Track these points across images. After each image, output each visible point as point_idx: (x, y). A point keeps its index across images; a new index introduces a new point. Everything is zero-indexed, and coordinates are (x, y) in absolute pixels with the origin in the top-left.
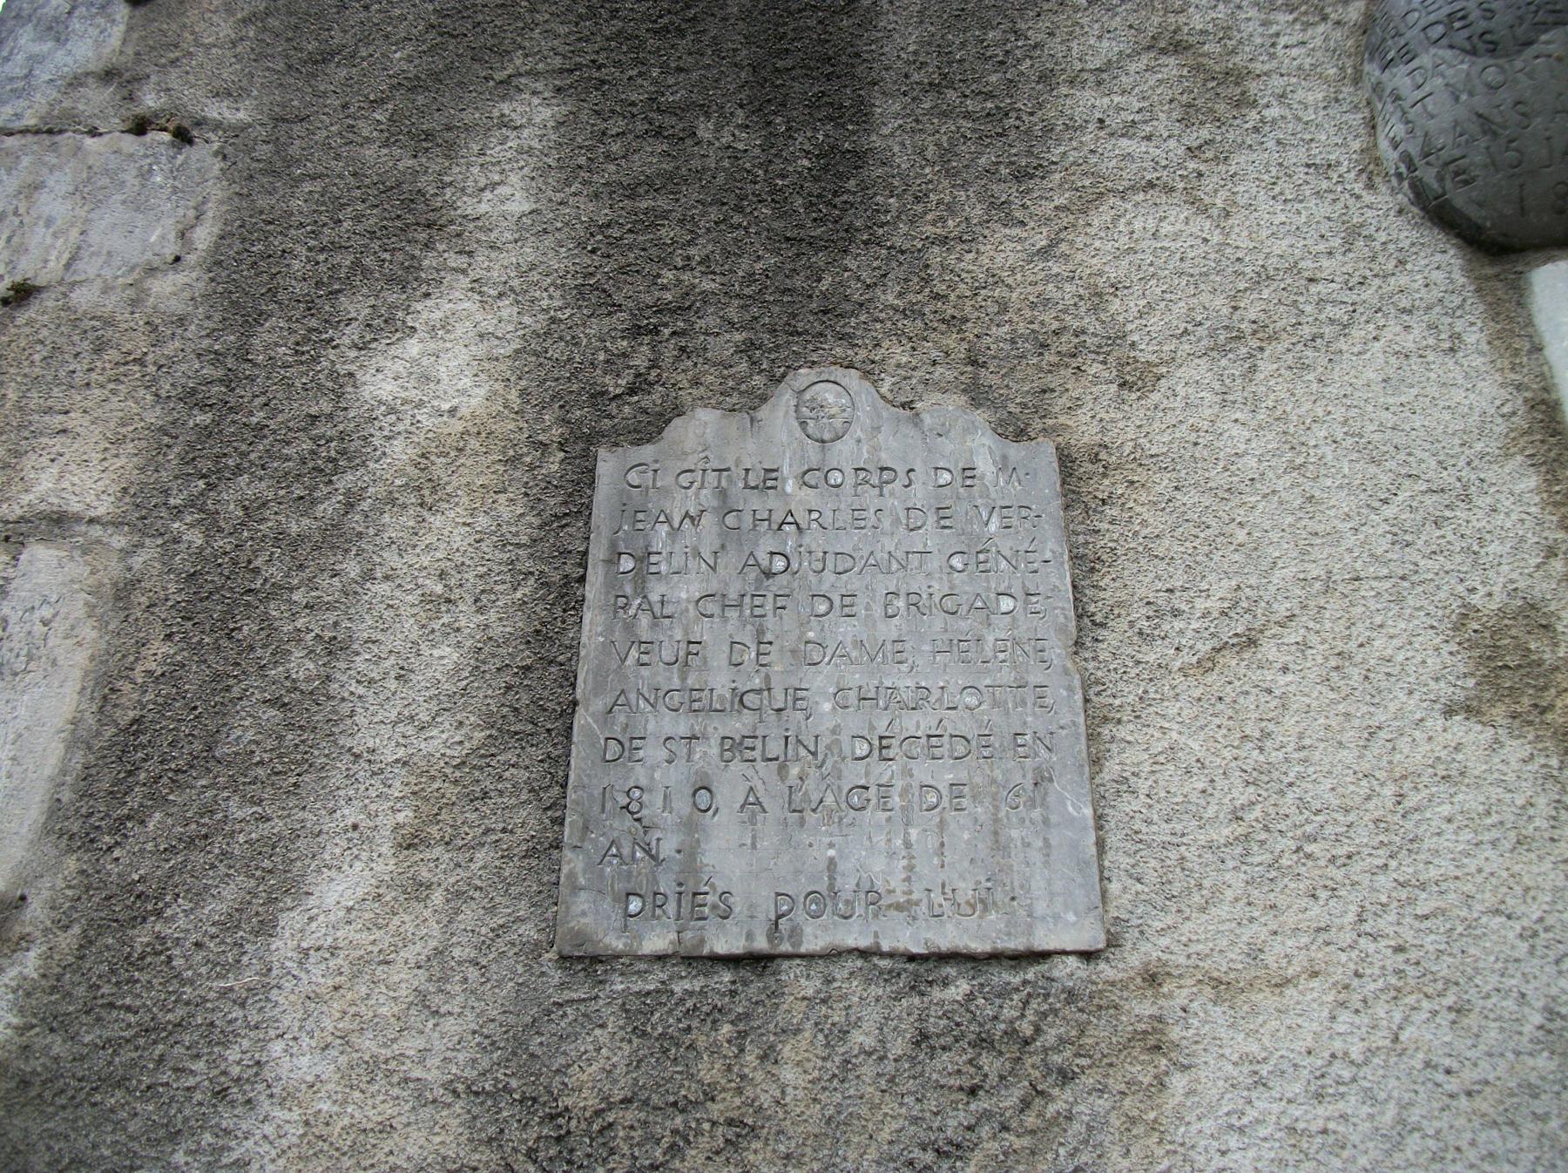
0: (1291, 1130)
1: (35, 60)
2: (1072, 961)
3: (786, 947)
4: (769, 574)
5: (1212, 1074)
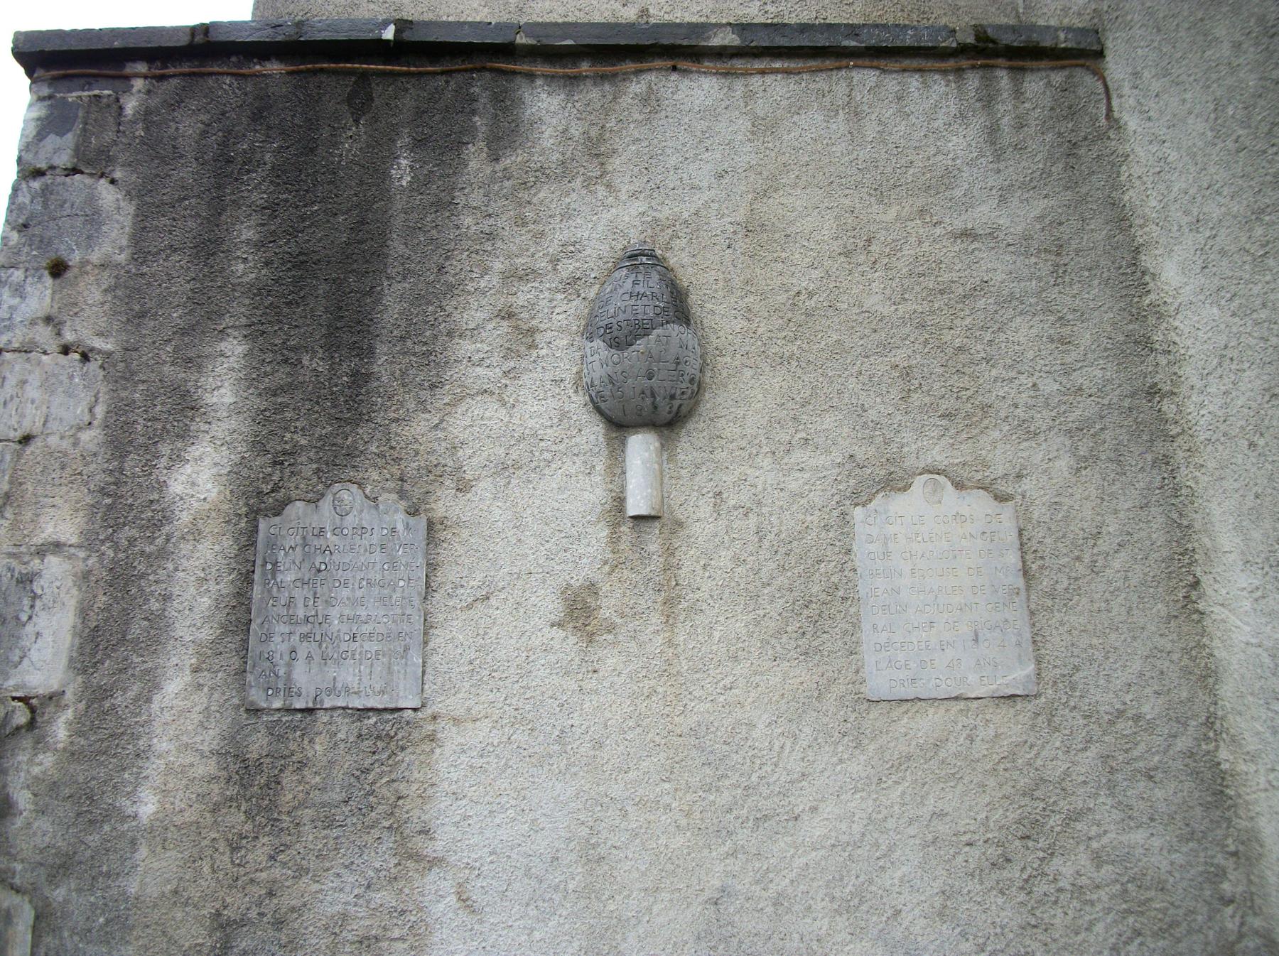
0: (471, 766)
1: (12, 309)
2: (410, 711)
3: (318, 706)
4: (319, 571)
5: (449, 748)
